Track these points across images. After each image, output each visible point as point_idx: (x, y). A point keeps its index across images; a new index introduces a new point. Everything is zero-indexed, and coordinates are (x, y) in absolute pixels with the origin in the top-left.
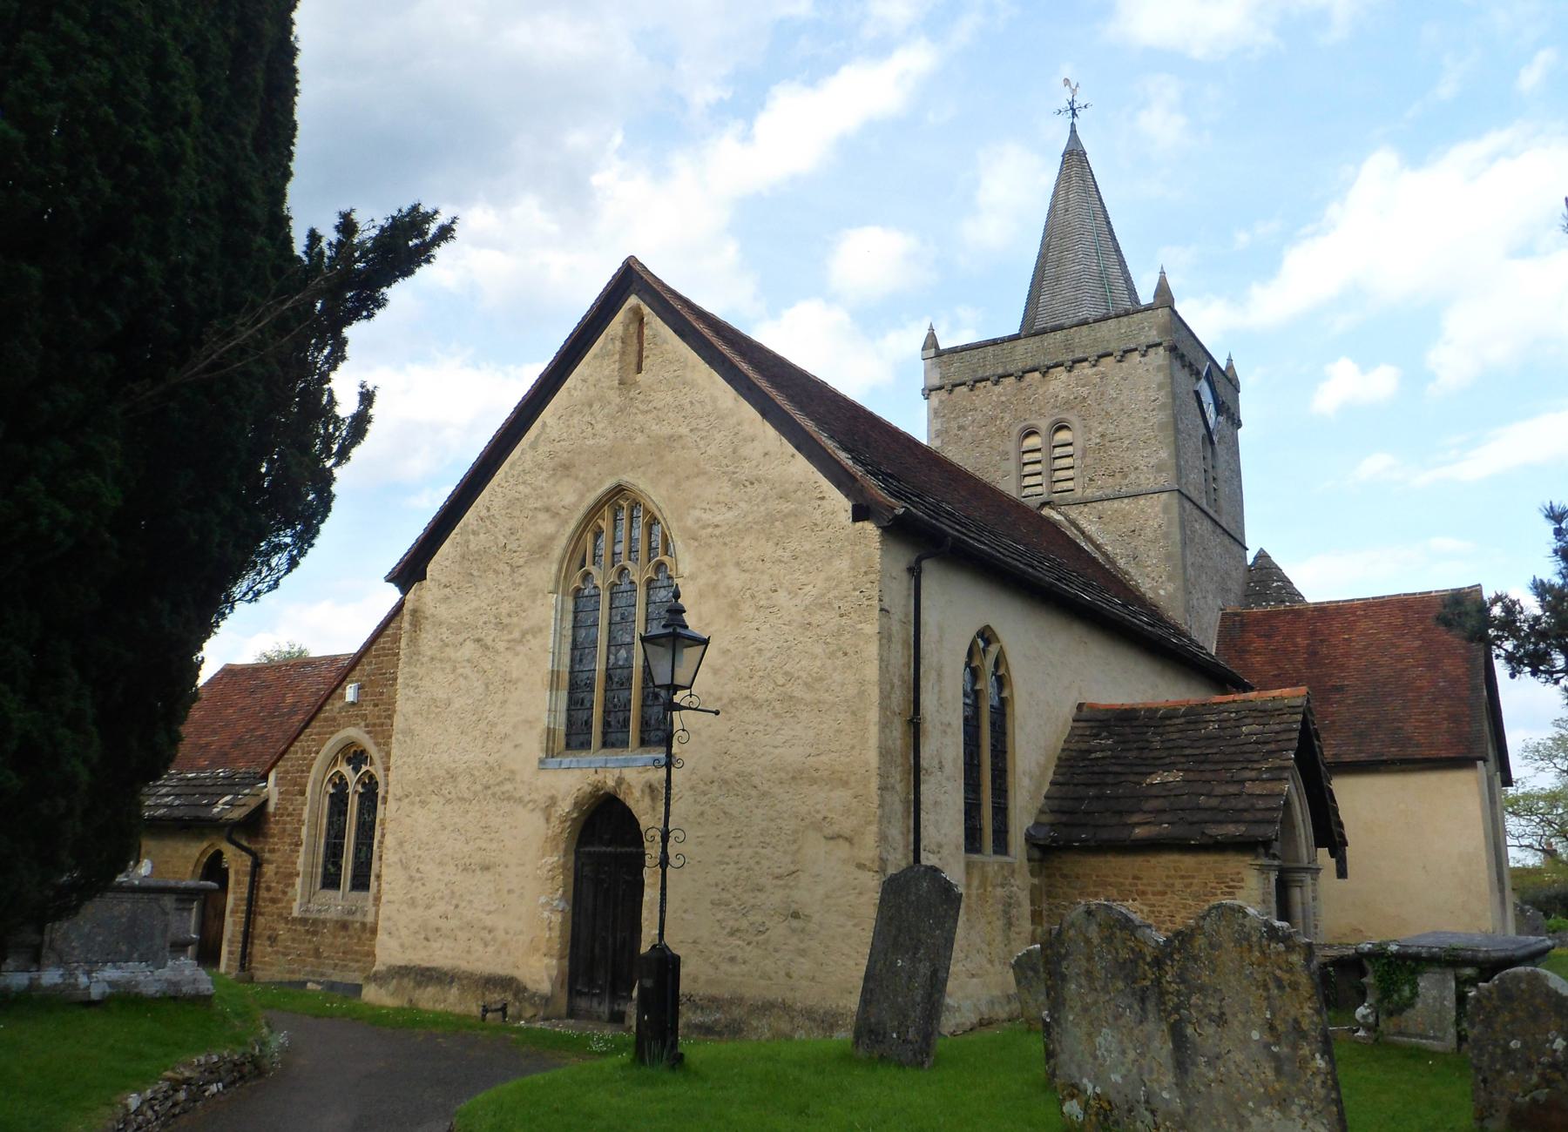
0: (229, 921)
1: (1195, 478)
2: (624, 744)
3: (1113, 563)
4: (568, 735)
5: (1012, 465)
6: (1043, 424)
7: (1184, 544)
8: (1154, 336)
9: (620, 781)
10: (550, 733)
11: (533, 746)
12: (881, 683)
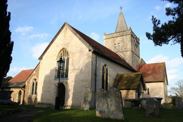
0: (21, 98)
1: (134, 50)
2: (63, 77)
3: (124, 59)
4: (57, 76)
5: (113, 48)
6: (117, 43)
7: (132, 57)
8: (129, 33)
9: (63, 82)
10: (55, 76)
11: (54, 78)
12: (91, 70)
